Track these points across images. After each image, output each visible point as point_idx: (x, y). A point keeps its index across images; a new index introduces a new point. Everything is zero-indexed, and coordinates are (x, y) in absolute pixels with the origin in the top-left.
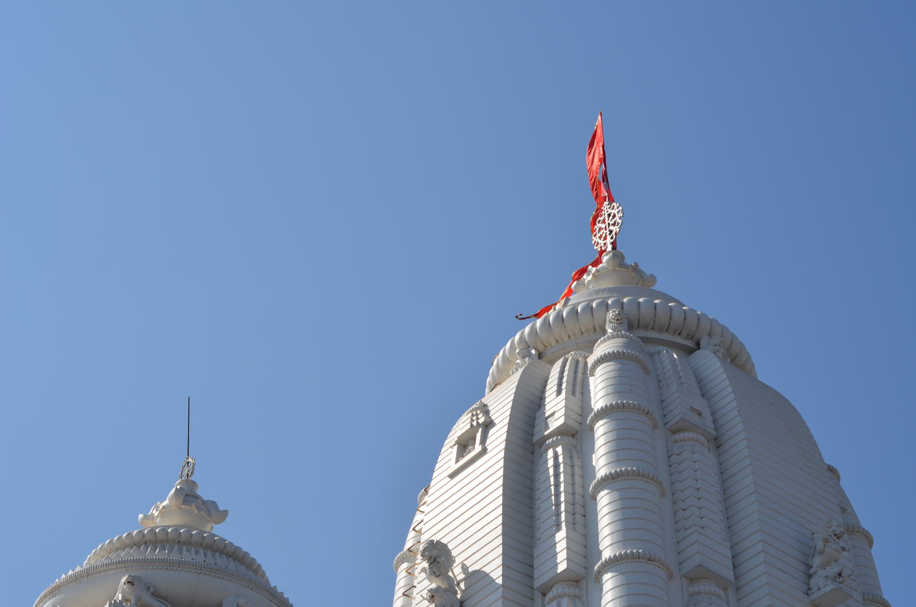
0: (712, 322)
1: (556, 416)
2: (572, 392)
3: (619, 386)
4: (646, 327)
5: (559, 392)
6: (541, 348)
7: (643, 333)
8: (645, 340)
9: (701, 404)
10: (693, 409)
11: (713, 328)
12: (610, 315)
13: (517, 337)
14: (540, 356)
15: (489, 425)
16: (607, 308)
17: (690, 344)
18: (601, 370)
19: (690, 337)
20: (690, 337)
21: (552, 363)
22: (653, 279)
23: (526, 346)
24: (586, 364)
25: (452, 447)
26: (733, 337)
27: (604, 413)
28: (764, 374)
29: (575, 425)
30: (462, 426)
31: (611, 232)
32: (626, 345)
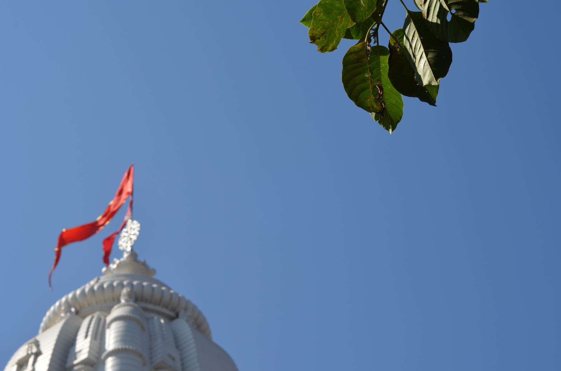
0: (188, 302)
1: (82, 352)
2: (94, 337)
3: (125, 337)
4: (146, 301)
5: (86, 337)
6: (78, 308)
7: (143, 305)
8: (145, 309)
9: (175, 353)
10: (170, 356)
11: (188, 306)
12: (125, 291)
13: (64, 299)
14: (77, 312)
15: (38, 354)
16: (121, 285)
17: (172, 314)
18: (114, 326)
19: (173, 310)
20: (173, 310)
21: (84, 317)
22: (154, 271)
23: (68, 305)
24: (105, 321)
25: (13, 366)
26: (200, 313)
27: (113, 353)
28: (218, 337)
29: (93, 359)
30: (21, 353)
31: (131, 239)
32: (132, 312)
